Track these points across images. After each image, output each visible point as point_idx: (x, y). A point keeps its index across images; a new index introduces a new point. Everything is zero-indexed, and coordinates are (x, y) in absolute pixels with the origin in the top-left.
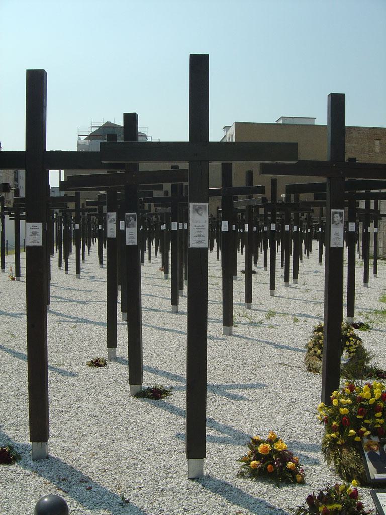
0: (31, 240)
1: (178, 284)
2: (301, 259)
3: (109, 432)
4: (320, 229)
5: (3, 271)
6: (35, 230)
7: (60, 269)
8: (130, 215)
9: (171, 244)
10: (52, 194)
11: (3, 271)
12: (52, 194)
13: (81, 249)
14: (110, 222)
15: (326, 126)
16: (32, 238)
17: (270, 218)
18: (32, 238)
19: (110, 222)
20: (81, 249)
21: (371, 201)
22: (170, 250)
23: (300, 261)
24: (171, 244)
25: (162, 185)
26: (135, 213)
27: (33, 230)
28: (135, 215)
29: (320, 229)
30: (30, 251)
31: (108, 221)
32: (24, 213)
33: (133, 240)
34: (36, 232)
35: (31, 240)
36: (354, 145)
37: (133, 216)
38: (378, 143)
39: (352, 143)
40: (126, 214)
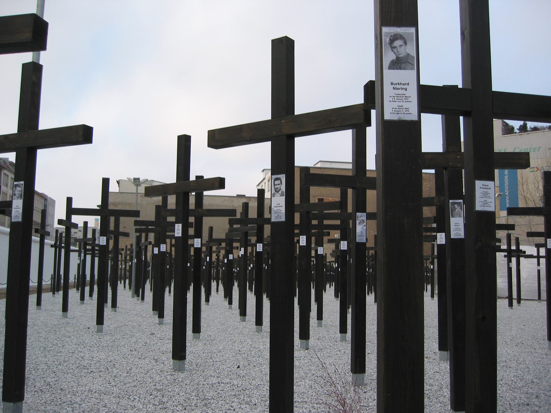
0: (482, 203)
1: (448, 274)
2: (325, 291)
7: (230, 308)
9: (248, 284)
10: (368, 175)
12: (368, 175)
14: (359, 223)
15: (310, 202)
16: (483, 200)
18: (483, 200)
19: (359, 223)
23: (323, 292)
24: (248, 284)
25: (193, 227)
26: (461, 201)
28: (460, 203)
31: (357, 222)
34: (487, 193)
35: (482, 203)
37: (458, 204)
40: (451, 201)
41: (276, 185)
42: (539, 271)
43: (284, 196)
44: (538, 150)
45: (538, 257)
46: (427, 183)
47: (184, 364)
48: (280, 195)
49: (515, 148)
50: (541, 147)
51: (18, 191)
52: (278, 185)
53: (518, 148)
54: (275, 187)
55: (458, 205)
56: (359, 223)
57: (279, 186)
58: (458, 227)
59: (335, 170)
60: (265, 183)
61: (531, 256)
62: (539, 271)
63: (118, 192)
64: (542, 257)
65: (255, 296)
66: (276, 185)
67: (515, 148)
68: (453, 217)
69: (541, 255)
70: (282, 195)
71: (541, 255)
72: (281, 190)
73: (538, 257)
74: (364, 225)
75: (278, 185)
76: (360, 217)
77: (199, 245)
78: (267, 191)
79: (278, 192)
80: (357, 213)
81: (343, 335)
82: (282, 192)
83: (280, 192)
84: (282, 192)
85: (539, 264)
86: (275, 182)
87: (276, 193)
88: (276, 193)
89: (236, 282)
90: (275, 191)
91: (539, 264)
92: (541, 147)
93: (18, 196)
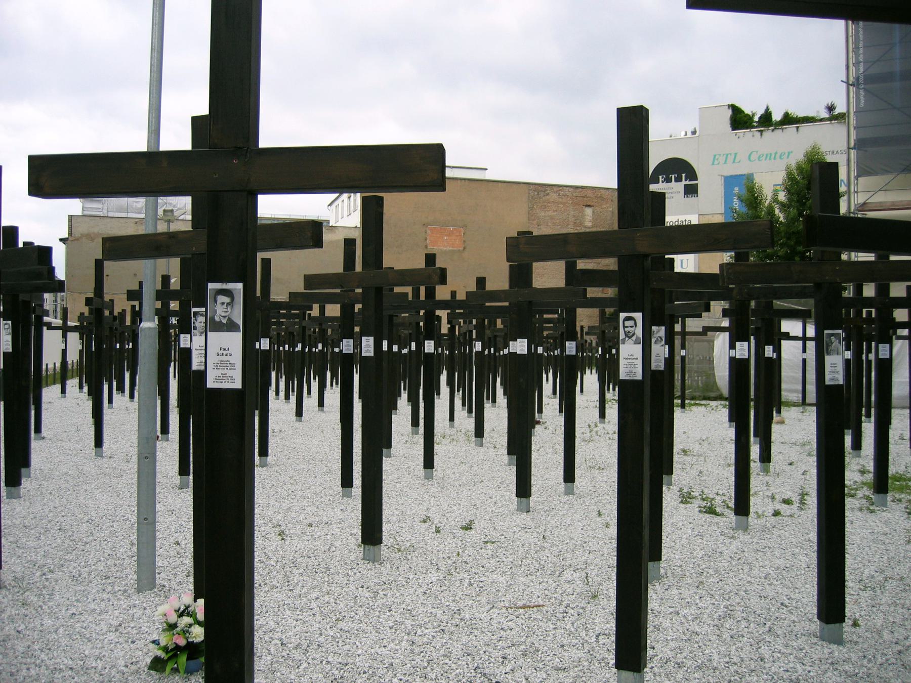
2: (439, 394)
3: (464, 663)
4: (320, 346)
5: (99, 455)
6: (631, 361)
8: (833, 335)
11: (99, 455)
13: (873, 379)
14: (656, 343)
17: (174, 321)
19: (656, 343)
20: (873, 379)
21: (424, 299)
22: (422, 387)
27: (629, 361)
28: (839, 334)
29: (320, 346)
30: (628, 390)
31: (653, 340)
32: (545, 333)
33: (229, 373)
36: (550, 213)
38: (589, 211)
39: (548, 211)
40: (826, 332)
41: (627, 327)
42: (804, 361)
43: (640, 343)
44: (788, 157)
45: (804, 339)
46: (608, 205)
47: (380, 549)
48: (633, 342)
49: (751, 153)
50: (792, 152)
51: (201, 322)
52: (631, 327)
53: (755, 153)
54: (626, 329)
55: (835, 337)
56: (656, 341)
57: (633, 329)
58: (835, 368)
59: (459, 181)
60: (343, 201)
61: (795, 338)
62: (804, 361)
63: (80, 214)
64: (811, 339)
65: (361, 400)
66: (627, 327)
67: (751, 153)
68: (828, 354)
69: (808, 336)
70: (636, 342)
71: (808, 336)
72: (635, 336)
73: (804, 339)
74: (662, 344)
75: (631, 327)
76: (657, 332)
77: (350, 350)
78: (347, 215)
79: (630, 337)
80: (653, 327)
81: (569, 484)
82: (637, 338)
83: (634, 338)
84: (637, 338)
85: (804, 351)
86: (626, 322)
87: (627, 339)
88: (627, 339)
89: (315, 378)
90: (626, 335)
91: (804, 351)
92: (792, 152)
93: (201, 331)
